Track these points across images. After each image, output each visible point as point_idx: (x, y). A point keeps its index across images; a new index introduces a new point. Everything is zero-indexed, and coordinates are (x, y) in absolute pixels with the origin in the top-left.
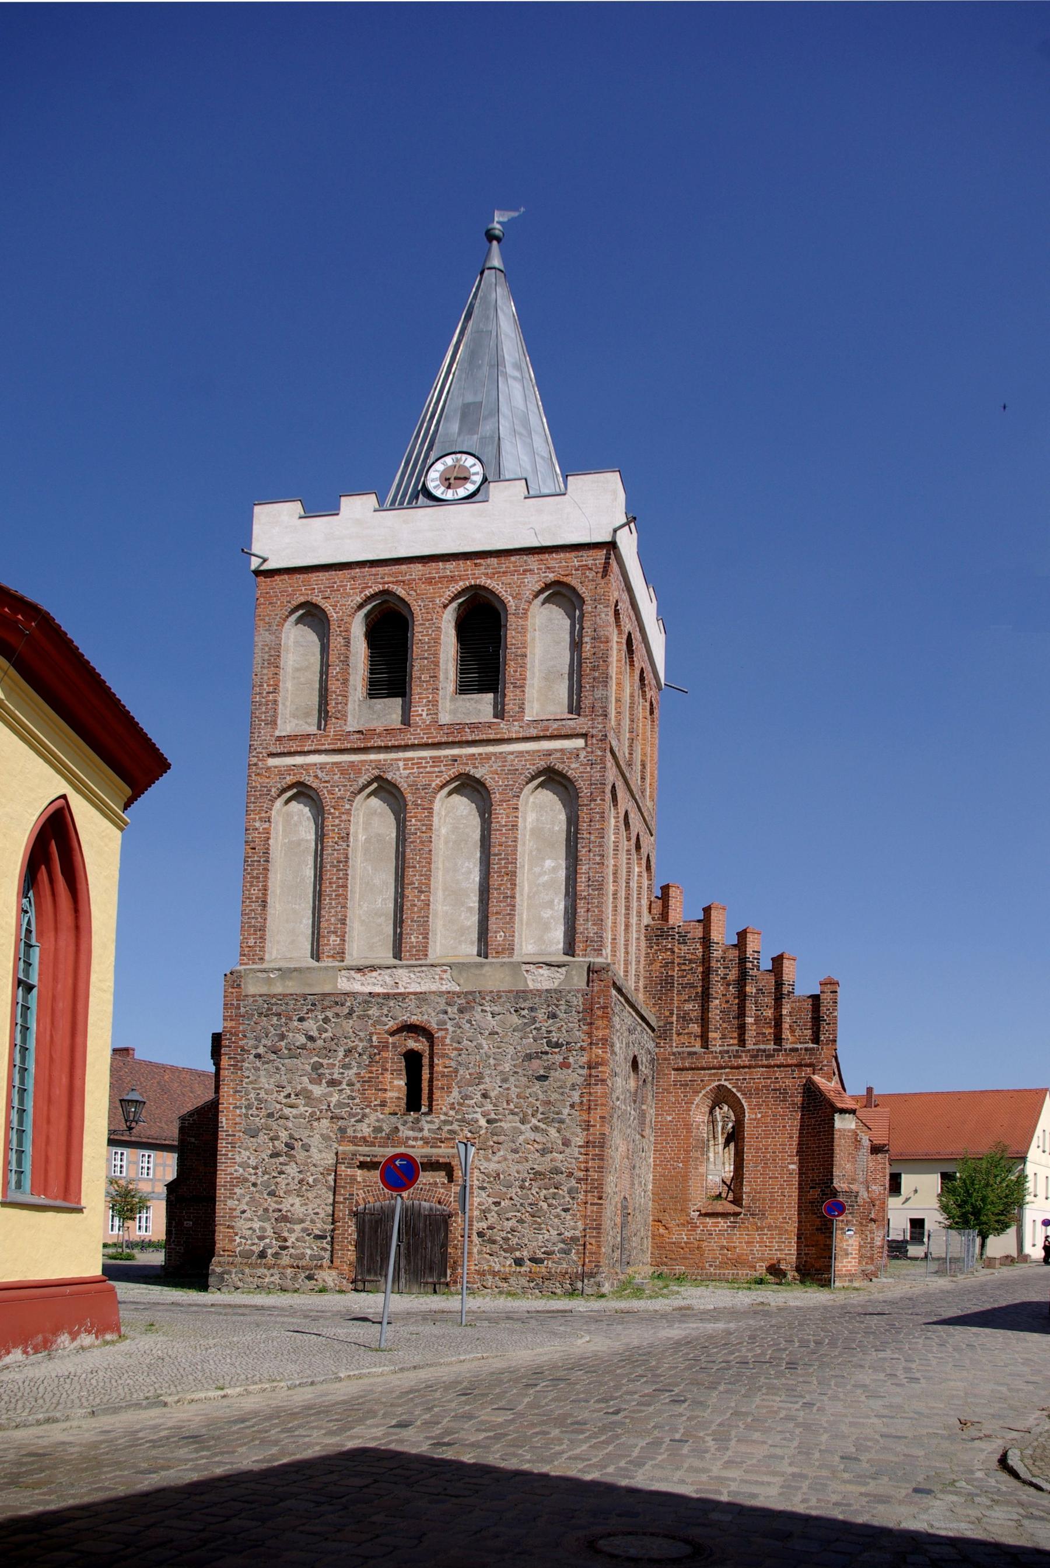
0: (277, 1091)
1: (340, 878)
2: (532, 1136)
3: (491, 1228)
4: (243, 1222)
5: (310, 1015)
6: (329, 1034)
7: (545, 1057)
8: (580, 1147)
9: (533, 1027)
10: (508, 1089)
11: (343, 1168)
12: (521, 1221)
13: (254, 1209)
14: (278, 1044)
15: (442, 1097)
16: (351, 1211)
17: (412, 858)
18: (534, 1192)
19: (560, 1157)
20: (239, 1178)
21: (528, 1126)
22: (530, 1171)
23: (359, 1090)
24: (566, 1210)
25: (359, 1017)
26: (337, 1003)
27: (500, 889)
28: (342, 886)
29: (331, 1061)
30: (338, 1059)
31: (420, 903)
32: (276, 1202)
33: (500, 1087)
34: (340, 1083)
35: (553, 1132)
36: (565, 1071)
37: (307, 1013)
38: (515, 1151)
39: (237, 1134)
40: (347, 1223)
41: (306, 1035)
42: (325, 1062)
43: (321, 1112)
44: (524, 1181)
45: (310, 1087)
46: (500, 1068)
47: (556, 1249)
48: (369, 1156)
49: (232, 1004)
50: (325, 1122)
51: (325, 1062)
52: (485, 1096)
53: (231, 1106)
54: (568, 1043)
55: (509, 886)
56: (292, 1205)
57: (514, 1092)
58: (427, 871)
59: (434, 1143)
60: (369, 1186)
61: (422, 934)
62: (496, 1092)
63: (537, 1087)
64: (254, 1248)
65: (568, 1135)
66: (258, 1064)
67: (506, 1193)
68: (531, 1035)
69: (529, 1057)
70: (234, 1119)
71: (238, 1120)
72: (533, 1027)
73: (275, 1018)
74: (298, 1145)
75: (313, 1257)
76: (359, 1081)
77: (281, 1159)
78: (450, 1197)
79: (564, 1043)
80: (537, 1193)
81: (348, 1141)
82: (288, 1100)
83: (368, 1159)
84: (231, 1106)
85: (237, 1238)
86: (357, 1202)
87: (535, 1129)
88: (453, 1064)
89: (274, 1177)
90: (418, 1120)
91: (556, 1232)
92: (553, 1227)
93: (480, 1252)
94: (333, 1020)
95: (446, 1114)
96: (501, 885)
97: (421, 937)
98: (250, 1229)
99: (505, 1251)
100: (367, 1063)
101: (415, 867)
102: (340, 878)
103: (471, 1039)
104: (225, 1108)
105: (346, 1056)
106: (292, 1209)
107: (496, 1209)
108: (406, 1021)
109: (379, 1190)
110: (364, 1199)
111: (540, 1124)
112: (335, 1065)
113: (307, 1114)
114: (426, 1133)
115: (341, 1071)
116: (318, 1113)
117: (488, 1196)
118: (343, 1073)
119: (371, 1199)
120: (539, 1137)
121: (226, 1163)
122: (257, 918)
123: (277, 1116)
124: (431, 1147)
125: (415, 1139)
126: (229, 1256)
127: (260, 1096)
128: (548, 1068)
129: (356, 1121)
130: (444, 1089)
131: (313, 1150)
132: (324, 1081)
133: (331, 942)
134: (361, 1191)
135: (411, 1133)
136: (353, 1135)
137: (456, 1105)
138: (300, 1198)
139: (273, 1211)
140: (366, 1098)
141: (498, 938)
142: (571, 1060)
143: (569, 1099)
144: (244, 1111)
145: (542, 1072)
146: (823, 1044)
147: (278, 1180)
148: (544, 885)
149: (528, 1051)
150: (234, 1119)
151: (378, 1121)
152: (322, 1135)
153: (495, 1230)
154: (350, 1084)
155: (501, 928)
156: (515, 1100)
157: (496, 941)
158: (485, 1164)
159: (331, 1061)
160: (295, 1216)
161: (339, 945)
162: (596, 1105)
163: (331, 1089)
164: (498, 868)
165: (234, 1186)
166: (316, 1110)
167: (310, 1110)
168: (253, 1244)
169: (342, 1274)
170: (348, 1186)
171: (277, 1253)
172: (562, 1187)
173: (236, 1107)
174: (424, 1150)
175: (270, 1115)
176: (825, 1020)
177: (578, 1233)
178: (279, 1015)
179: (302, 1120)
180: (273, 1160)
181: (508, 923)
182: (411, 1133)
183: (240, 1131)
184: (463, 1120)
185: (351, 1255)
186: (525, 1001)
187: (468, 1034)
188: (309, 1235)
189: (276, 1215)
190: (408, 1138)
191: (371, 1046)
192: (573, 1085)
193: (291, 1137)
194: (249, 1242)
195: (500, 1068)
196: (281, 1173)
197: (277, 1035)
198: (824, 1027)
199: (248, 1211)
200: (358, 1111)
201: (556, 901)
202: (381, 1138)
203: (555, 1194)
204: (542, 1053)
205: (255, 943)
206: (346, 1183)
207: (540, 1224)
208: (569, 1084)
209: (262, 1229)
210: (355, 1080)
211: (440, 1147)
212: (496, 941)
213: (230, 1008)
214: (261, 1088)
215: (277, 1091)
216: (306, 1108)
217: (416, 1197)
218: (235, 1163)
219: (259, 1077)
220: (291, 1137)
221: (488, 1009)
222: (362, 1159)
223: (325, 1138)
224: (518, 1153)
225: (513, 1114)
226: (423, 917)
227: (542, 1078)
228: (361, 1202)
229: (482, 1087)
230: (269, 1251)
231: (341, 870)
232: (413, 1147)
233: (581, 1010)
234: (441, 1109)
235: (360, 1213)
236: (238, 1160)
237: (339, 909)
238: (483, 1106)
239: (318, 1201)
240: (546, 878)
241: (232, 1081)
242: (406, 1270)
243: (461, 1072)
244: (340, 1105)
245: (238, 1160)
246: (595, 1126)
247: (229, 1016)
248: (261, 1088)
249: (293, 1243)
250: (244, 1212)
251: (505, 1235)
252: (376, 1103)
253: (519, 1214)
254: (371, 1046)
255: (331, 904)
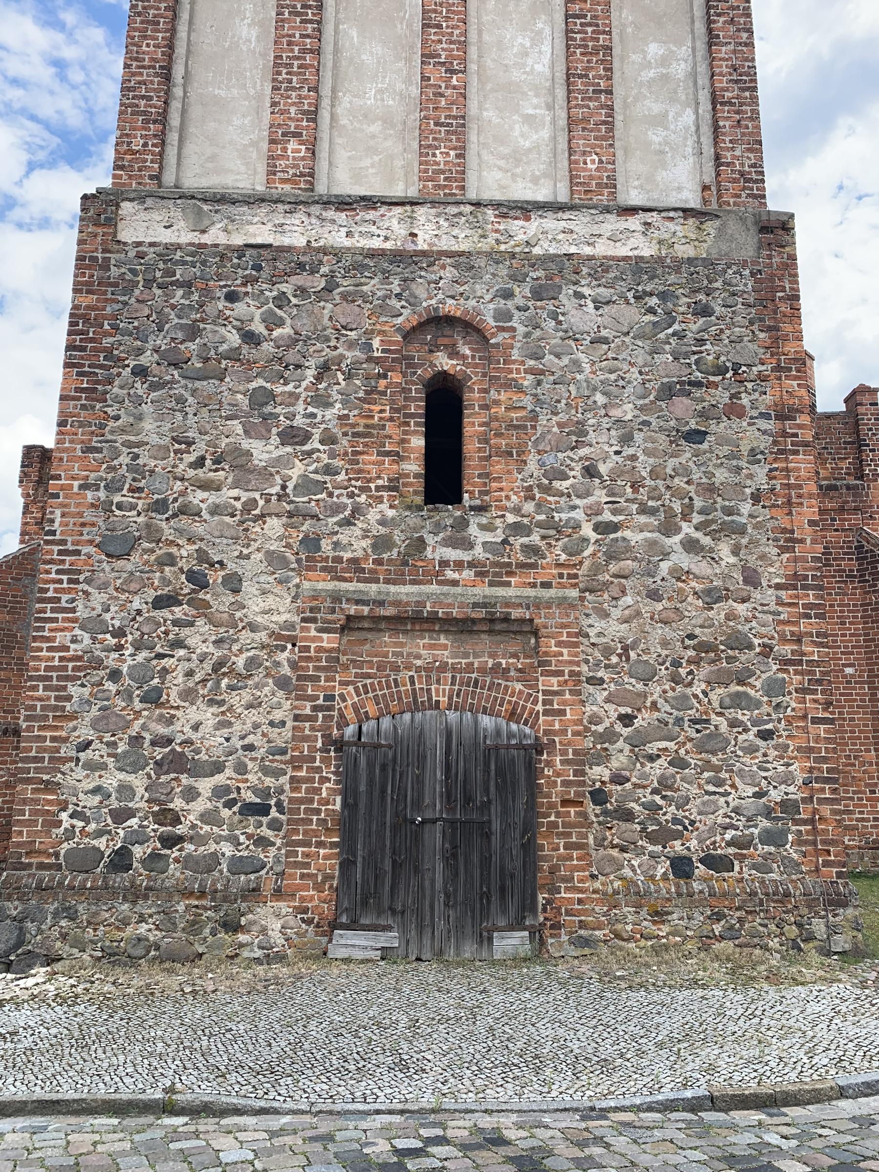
0: (176, 452)
1: (308, 36)
2: (683, 560)
3: (619, 779)
4: (80, 773)
5: (249, 289)
6: (285, 331)
7: (698, 393)
8: (778, 587)
9: (670, 331)
10: (633, 458)
11: (313, 633)
12: (679, 763)
13: (107, 738)
14: (182, 347)
15: (509, 472)
16: (328, 740)
17: (435, 11)
18: (698, 692)
19: (742, 609)
20: (79, 658)
21: (677, 539)
22: (688, 642)
23: (346, 454)
24: (765, 735)
25: (344, 296)
26: (301, 266)
27: (586, 76)
28: (311, 51)
29: (289, 388)
30: (304, 384)
31: (449, 91)
32: (161, 719)
33: (617, 453)
34: (307, 437)
35: (724, 550)
36: (736, 423)
37: (244, 285)
38: (654, 595)
39: (86, 550)
40: (319, 770)
41: (239, 330)
42: (279, 389)
43: (268, 501)
44: (677, 664)
45: (246, 444)
46: (616, 413)
47: (756, 831)
48: (365, 603)
49: (94, 259)
50: (274, 525)
51: (279, 389)
52: (590, 472)
53: (76, 484)
54: (736, 367)
55: (602, 72)
56: (196, 727)
57: (644, 465)
58: (461, 35)
59: (496, 574)
60: (368, 676)
61: (455, 149)
62: (610, 465)
63: (687, 453)
64: (101, 843)
65: (752, 561)
66: (140, 388)
67: (645, 695)
68: (667, 347)
69: (668, 392)
70: (81, 515)
71: (89, 516)
72: (670, 331)
73: (180, 292)
74: (216, 577)
75: (239, 866)
76: (345, 434)
77: (178, 612)
78: (535, 702)
79: (728, 364)
80: (705, 693)
81: (324, 569)
82: (200, 471)
83: (366, 610)
84: (76, 484)
85: (64, 816)
86: (342, 716)
87: (691, 546)
88: (527, 401)
89: (160, 656)
90: (462, 524)
91: (750, 791)
92: (742, 777)
93: (600, 843)
94: (294, 301)
95: (517, 510)
96: (588, 69)
97: (452, 153)
98: (97, 790)
99: (652, 838)
100: (361, 394)
101: (439, 26)
102: (308, 36)
103: (558, 350)
104: (62, 488)
105: (319, 378)
106: (194, 736)
107: (626, 731)
108: (436, 309)
109: (389, 687)
110: (356, 710)
111: (698, 535)
112: (297, 397)
113: (238, 505)
114: (479, 552)
115: (310, 409)
116: (261, 503)
117: (608, 700)
118: (313, 415)
119: (371, 709)
120: (702, 567)
121: (56, 620)
122: (150, 98)
123: (173, 507)
124: (491, 584)
125: (459, 565)
126: (42, 866)
127: (140, 461)
128: (703, 415)
129: (342, 524)
130: (510, 454)
131: (249, 588)
132: (274, 431)
133: (289, 153)
134: (351, 688)
135: (453, 554)
136: (331, 554)
137: (536, 490)
138: (214, 709)
139: (153, 743)
140: (360, 471)
141: (589, 166)
142: (745, 400)
143: (749, 482)
144: (102, 494)
145: (693, 425)
146: (869, 480)
147: (166, 662)
148: (650, 83)
149: (665, 380)
150: (81, 515)
151: (383, 522)
152: (269, 554)
153: (628, 786)
154: (328, 439)
155: (593, 147)
156: (648, 482)
157: (585, 170)
158: (599, 625)
159: (289, 388)
160: (203, 757)
161: (303, 159)
162: (799, 496)
163: (289, 449)
164: (582, 39)
165: (67, 678)
166: (257, 495)
167: (245, 496)
168: (99, 834)
169: (305, 911)
170: (322, 675)
171: (155, 856)
172: (751, 680)
173: (84, 487)
174: (477, 590)
175: (160, 506)
176: (868, 445)
177: (794, 792)
178: (187, 285)
179: (228, 519)
180: (159, 614)
181: (603, 138)
182: (453, 554)
183: (91, 542)
184: (550, 524)
185: (326, 857)
186: (651, 278)
187: (553, 342)
188: (229, 804)
189: (159, 753)
190: (444, 563)
191: (370, 359)
192: (753, 452)
193: (202, 557)
194: (93, 826)
195: (616, 413)
196: (179, 644)
197: (182, 327)
198: (868, 456)
199: (96, 745)
200: (344, 500)
201: (671, 115)
202: (390, 560)
203: (738, 694)
204: (690, 383)
205: (145, 145)
206: (317, 668)
207: (718, 769)
208: (745, 449)
209: (126, 790)
210: (337, 431)
211: (508, 584)
212: (585, 170)
213: (89, 267)
214: (139, 445)
215: (176, 452)
216: (235, 492)
217: (465, 701)
218: (75, 620)
219: (140, 418)
220: (202, 557)
221: (586, 291)
222: (352, 610)
223: (275, 560)
224: (659, 600)
225: (644, 510)
226: (455, 118)
227: (696, 436)
228: (350, 715)
229: (583, 452)
230: (138, 851)
231: (311, 22)
232: (455, 583)
233: (752, 300)
234: (508, 498)
235: (349, 744)
236: (82, 613)
237: (305, 92)
238: (588, 494)
239: (253, 716)
240: (652, 74)
241: (81, 425)
242: (447, 896)
243: (543, 420)
244: (306, 486)
245: (82, 613)
246: (802, 541)
247: (86, 283)
248: (139, 445)
249: (193, 827)
250: (85, 746)
251: (649, 797)
252: (380, 482)
253: (671, 745)
254: (370, 359)
255: (290, 81)
